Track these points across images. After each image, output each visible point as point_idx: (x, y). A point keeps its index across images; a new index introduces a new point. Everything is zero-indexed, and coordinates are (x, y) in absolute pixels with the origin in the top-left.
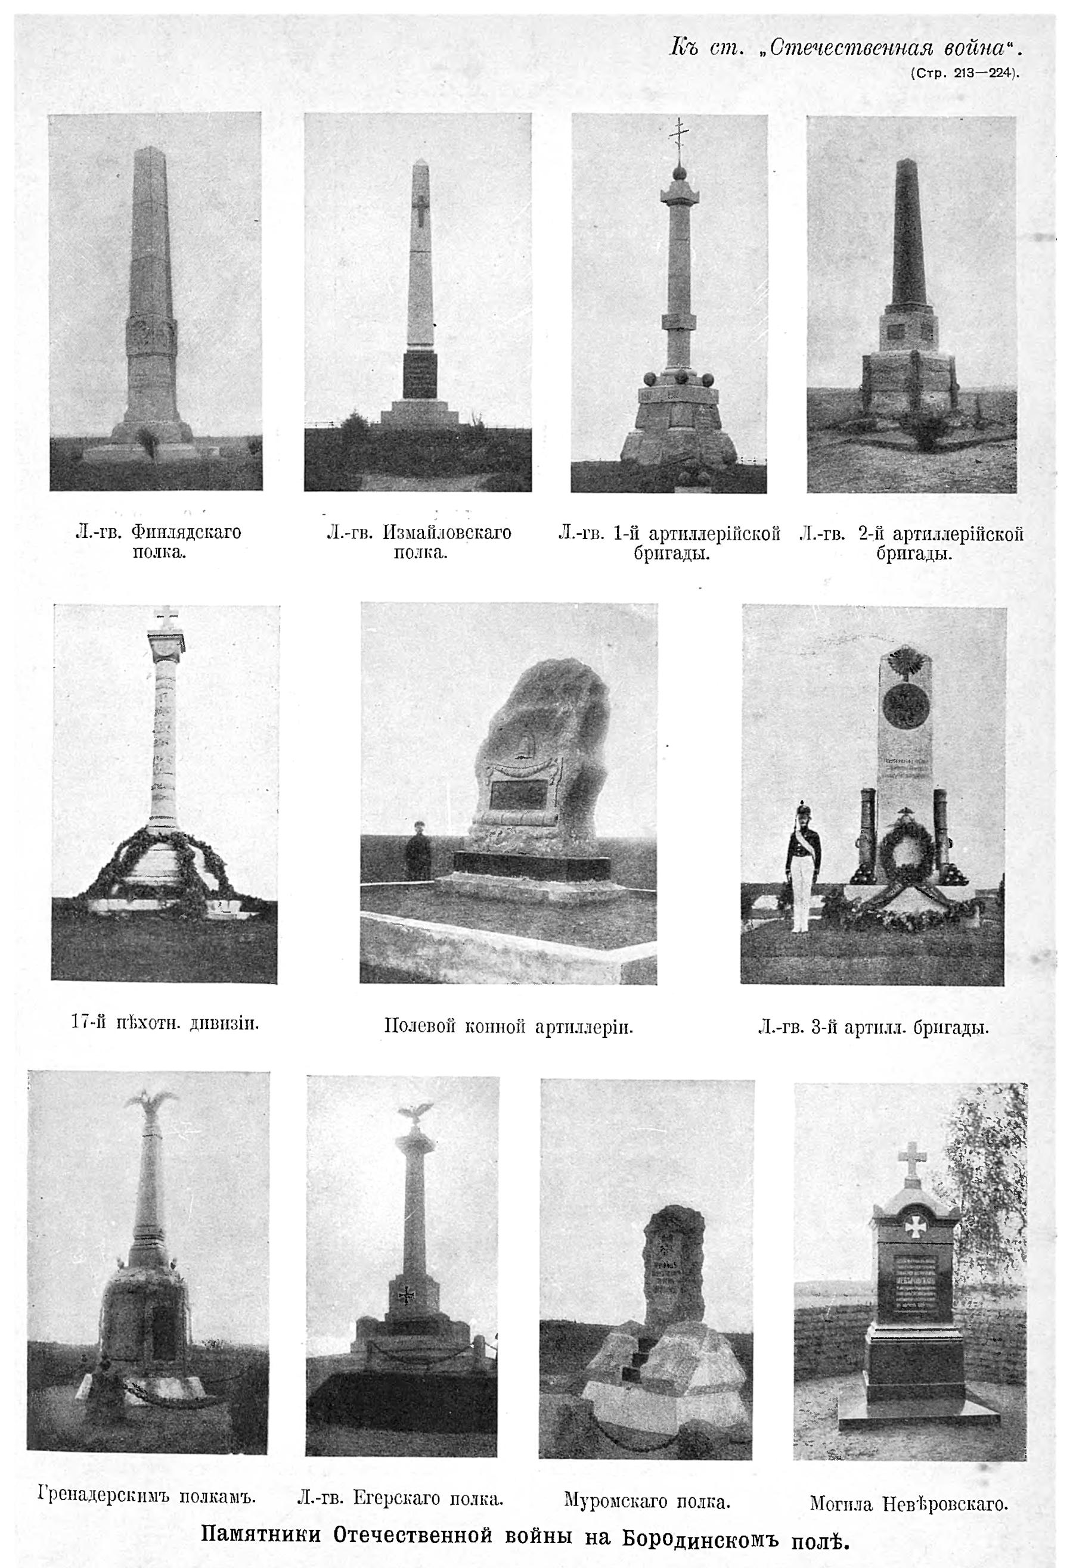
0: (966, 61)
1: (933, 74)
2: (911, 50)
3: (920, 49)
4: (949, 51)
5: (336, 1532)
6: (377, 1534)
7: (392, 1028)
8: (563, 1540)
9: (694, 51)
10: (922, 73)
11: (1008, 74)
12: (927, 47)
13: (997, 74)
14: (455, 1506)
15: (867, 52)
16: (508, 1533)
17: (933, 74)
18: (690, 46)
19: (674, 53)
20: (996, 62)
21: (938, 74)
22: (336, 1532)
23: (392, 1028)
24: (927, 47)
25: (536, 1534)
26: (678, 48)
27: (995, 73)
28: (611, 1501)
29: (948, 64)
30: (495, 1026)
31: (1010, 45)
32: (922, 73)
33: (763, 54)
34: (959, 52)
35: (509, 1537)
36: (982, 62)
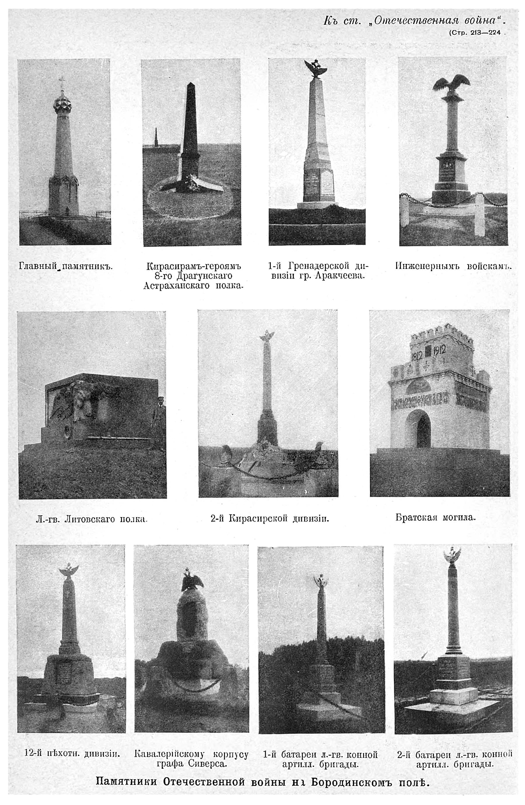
0: (476, 27)
1: (460, 33)
4: (467, 22)
9: (335, 23)
13: (493, 33)
21: (463, 33)
24: (456, 20)
26: (327, 21)
29: (468, 28)
33: (371, 24)
35: (253, 783)
36: (485, 27)
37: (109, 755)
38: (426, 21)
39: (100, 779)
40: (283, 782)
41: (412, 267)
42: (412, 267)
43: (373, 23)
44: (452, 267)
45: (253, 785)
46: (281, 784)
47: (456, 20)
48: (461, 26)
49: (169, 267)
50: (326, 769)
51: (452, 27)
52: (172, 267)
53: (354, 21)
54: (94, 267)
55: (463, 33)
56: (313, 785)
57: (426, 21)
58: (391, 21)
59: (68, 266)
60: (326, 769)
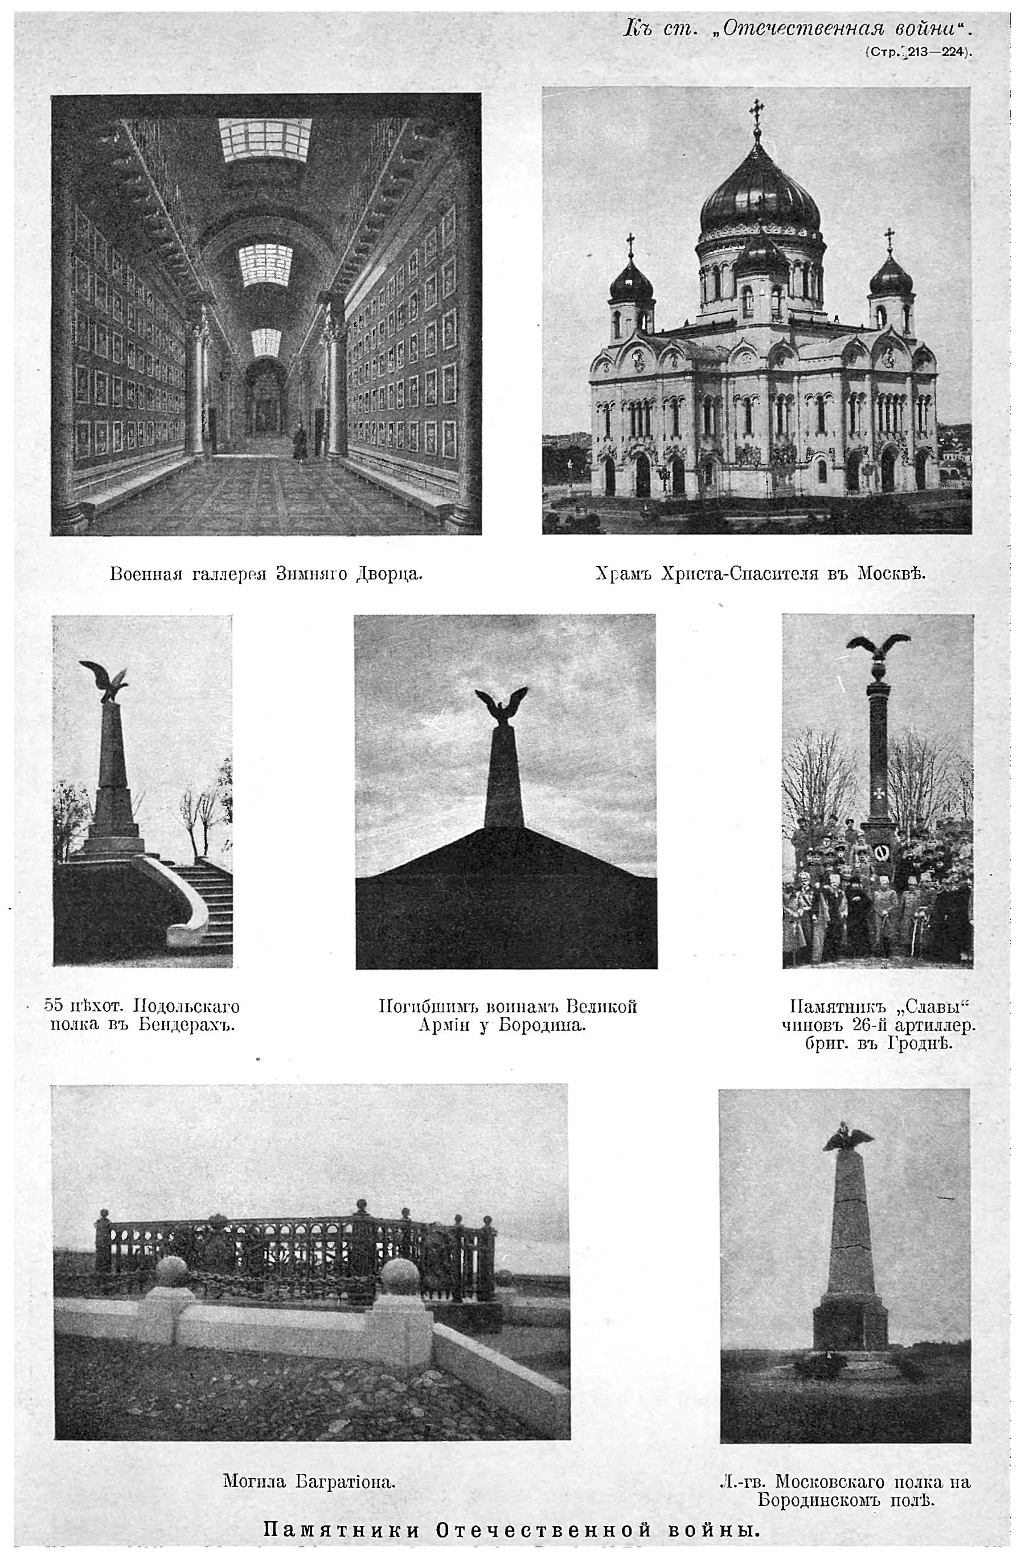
0: (917, 41)
1: (887, 53)
2: (865, 30)
3: (871, 29)
4: (900, 31)
5: (438, 1527)
6: (493, 1529)
7: (386, 1008)
8: (743, 1533)
9: (648, 32)
10: (876, 51)
11: (961, 53)
12: (878, 27)
13: (950, 53)
14: (896, 1507)
15: (818, 31)
16: (555, 1527)
17: (887, 53)
18: (644, 27)
19: (628, 34)
20: (945, 41)
21: (892, 53)
22: (438, 1527)
23: (386, 1008)
24: (878, 27)
25: (644, 1528)
26: (632, 30)
27: (947, 52)
28: (860, 1500)
29: (900, 43)
30: (803, 1028)
31: (961, 25)
32: (876, 51)
33: (716, 34)
34: (910, 32)
35: (555, 1531)
36: (934, 42)
37: (375, 1483)
38: (822, 29)
39: (270, 1525)
40: (747, 1530)
41: (304, 575)
42: (304, 575)
43: (722, 32)
44: (636, 576)
45: (555, 1536)
46: (743, 1533)
47: (880, 29)
48: (889, 40)
49: (762, 575)
50: (783, 1509)
51: (876, 41)
52: (768, 575)
53: (682, 29)
54: (152, 577)
55: (892, 53)
56: (741, 1535)
57: (822, 29)
58: (755, 29)
59: (753, 574)
60: (783, 1509)
